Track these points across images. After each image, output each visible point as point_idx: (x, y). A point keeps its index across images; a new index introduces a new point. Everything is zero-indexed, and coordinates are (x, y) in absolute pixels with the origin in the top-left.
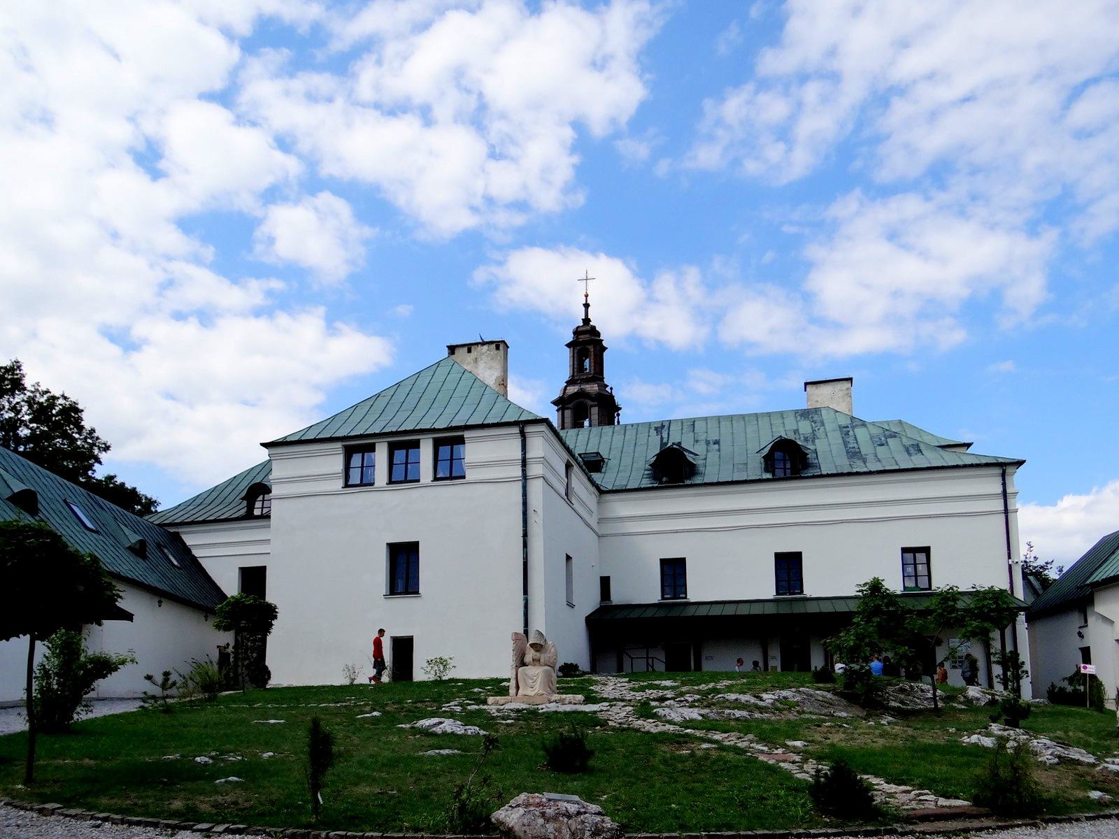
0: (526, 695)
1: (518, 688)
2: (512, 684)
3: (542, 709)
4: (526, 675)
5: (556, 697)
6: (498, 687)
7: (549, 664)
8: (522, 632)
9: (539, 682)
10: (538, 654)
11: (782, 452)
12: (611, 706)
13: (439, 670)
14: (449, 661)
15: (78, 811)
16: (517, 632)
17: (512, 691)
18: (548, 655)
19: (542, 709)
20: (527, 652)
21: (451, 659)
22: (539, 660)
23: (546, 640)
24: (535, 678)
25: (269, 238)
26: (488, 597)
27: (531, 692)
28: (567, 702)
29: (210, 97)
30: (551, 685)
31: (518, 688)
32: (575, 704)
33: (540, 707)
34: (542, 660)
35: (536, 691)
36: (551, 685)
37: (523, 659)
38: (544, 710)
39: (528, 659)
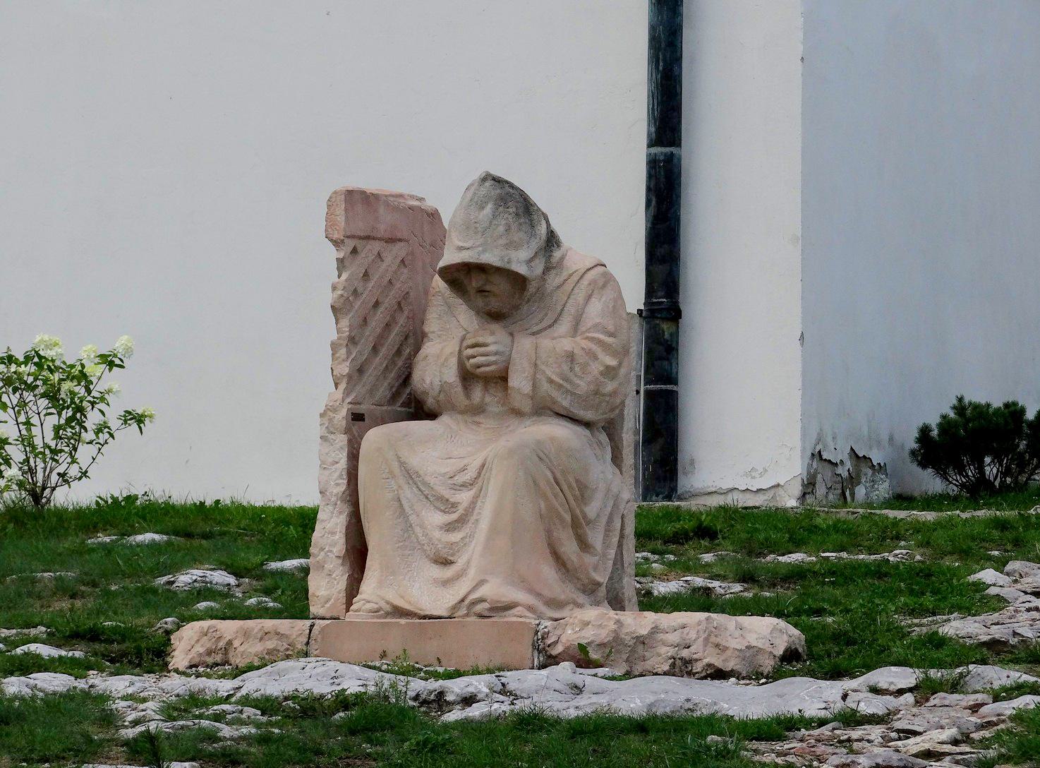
0: (399, 612)
1: (358, 554)
2: (329, 535)
3: (468, 701)
4: (411, 476)
5: (589, 623)
6: (257, 549)
7: (565, 402)
8: (636, 313)
9: (484, 525)
10: (494, 339)
11: (61, 514)
12: (924, 691)
13: (27, 442)
14: (105, 380)
15: (659, 98)
16: (370, 186)
17: (325, 586)
18: (566, 344)
19: (468, 701)
20: (432, 325)
21: (109, 361)
22: (502, 378)
23: (552, 240)
24: (464, 497)
25: (494, 333)
26: (901, 764)
27: (427, 592)
28: (660, 657)
29: (506, 388)
30: (569, 548)
31: (358, 554)
32: (719, 674)
33: (455, 688)
34: (519, 381)
35: (461, 589)
36: (569, 548)
37: (406, 379)
38: (475, 711)
39: (435, 368)
